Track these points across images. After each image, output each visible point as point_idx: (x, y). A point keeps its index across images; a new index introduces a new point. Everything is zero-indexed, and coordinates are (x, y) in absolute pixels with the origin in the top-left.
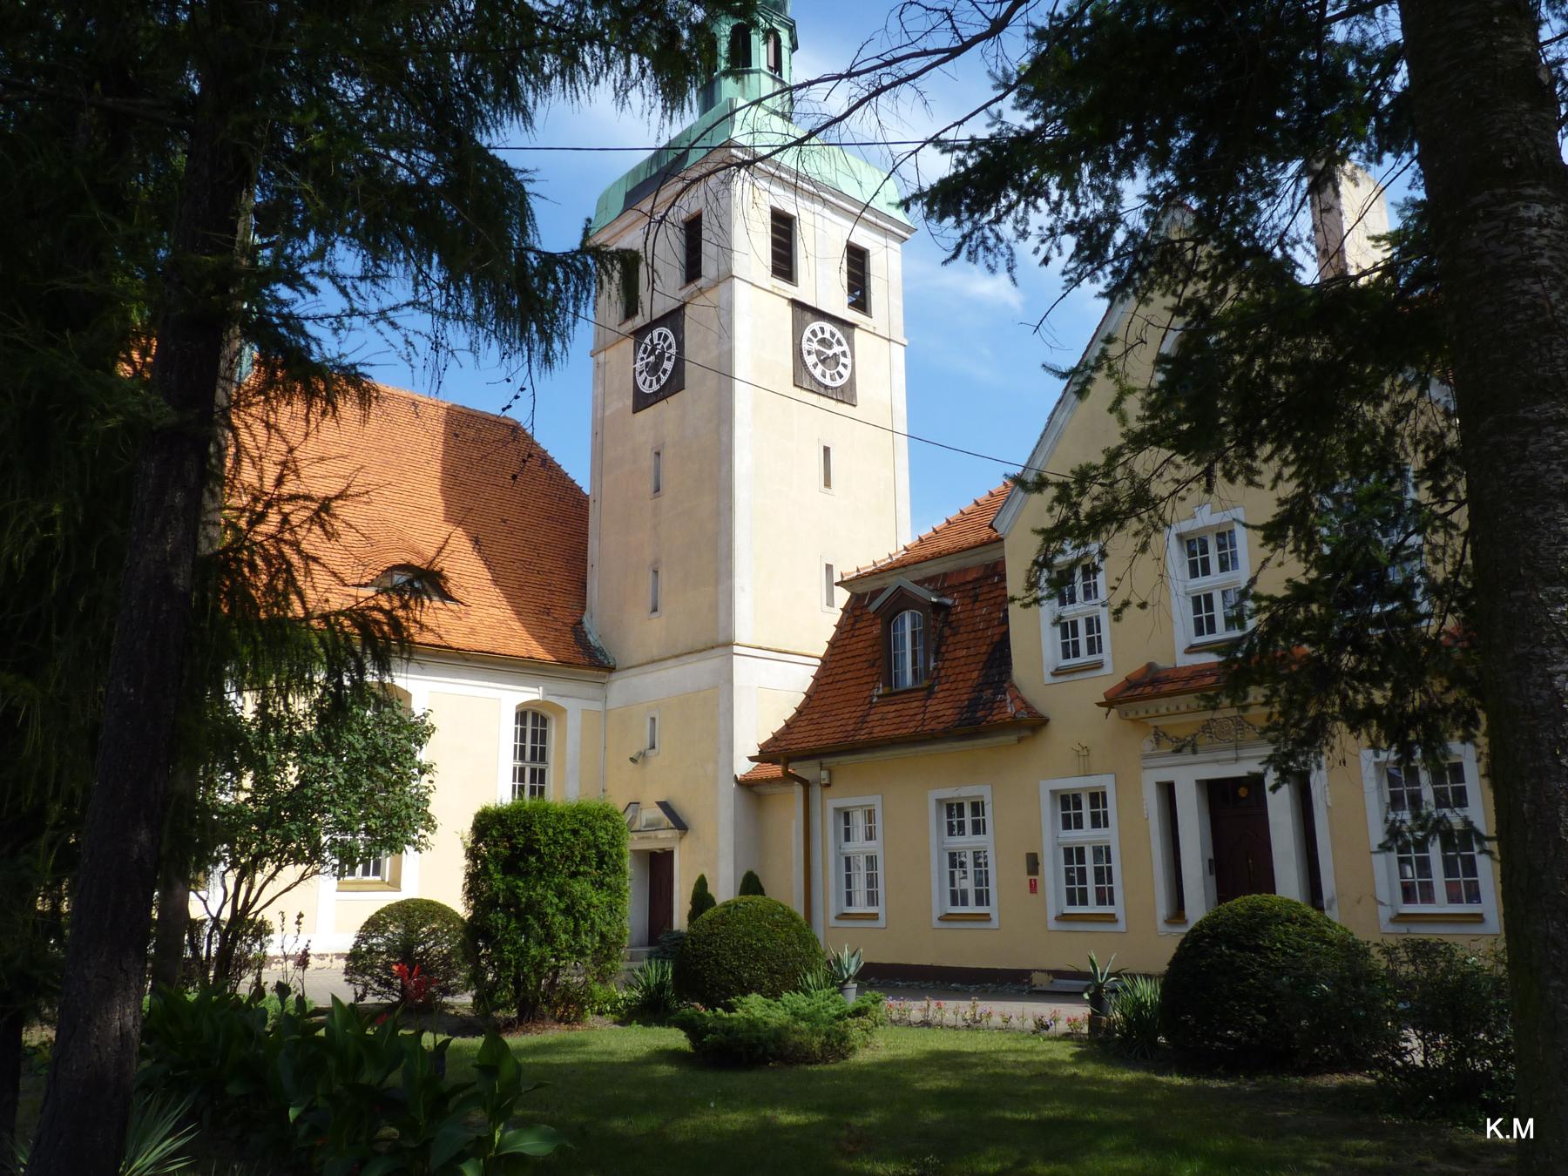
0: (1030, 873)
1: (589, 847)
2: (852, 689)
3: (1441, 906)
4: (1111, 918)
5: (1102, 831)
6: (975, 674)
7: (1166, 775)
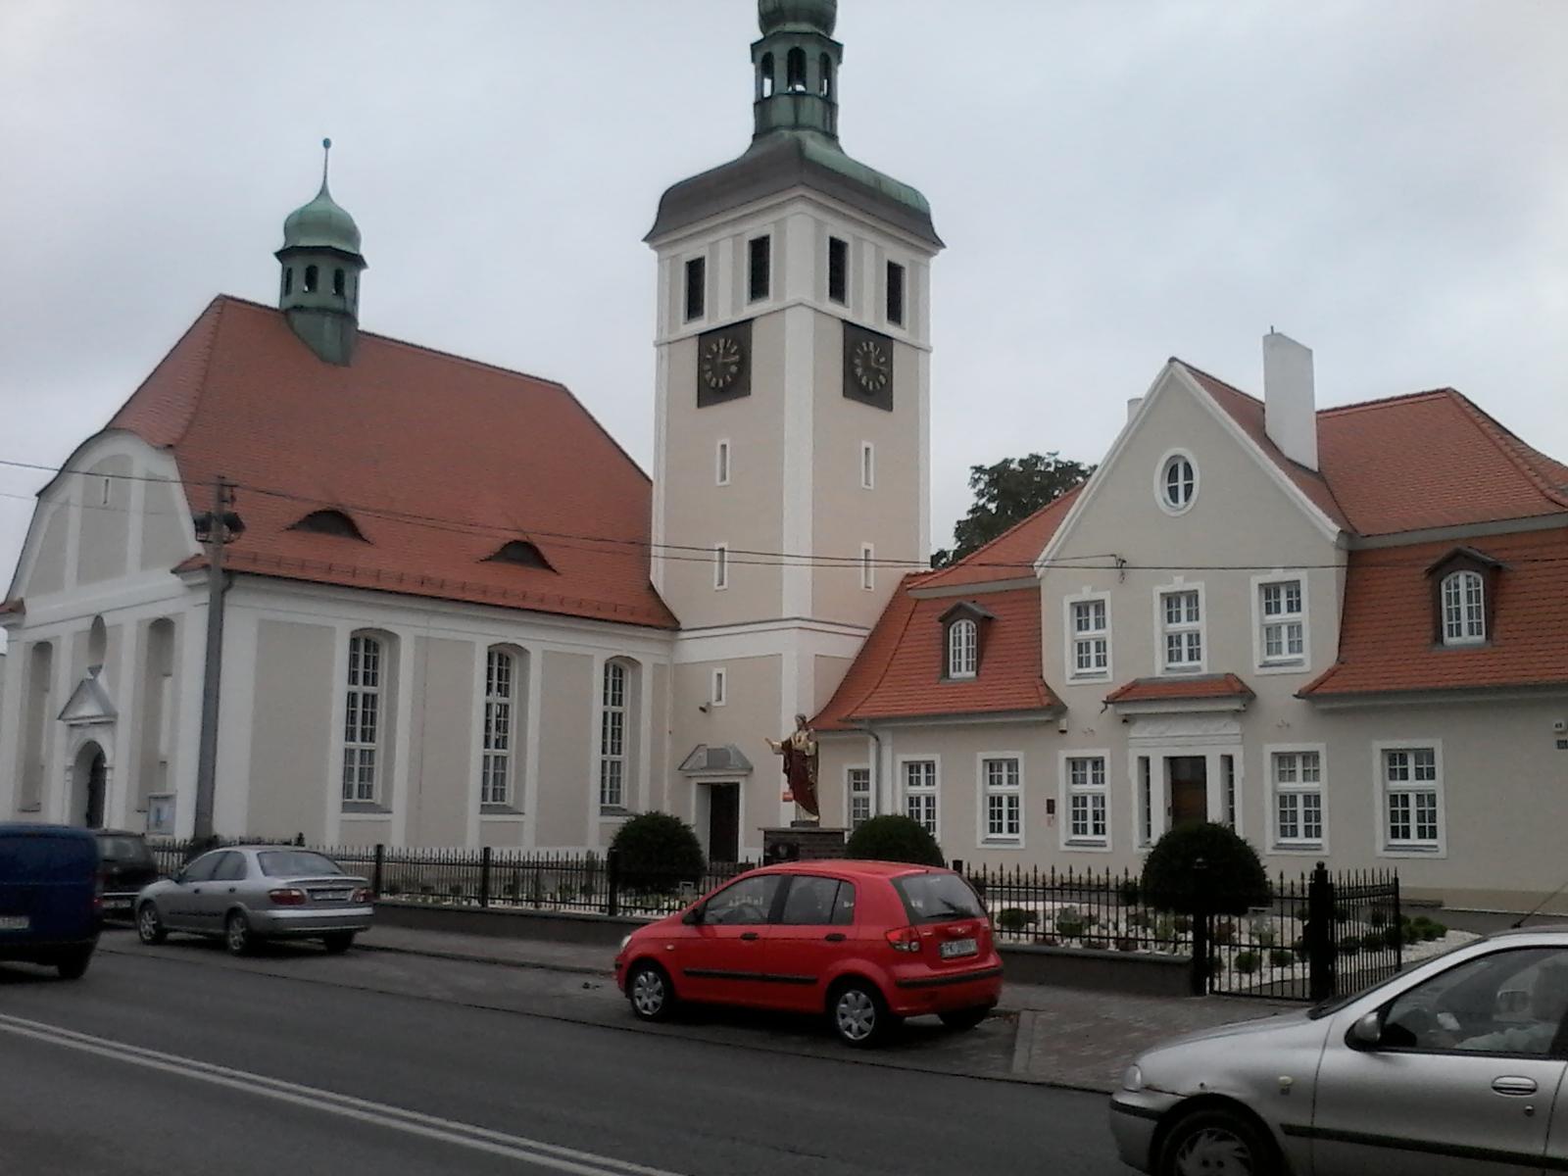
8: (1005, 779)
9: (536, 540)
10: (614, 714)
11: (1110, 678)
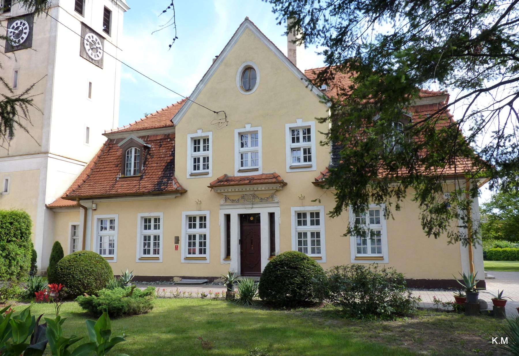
0: (176, 243)
1: (17, 230)
2: (108, 174)
3: (369, 254)
4: (204, 259)
5: (157, 231)
6: (160, 173)
7: (227, 212)
8: (198, 225)
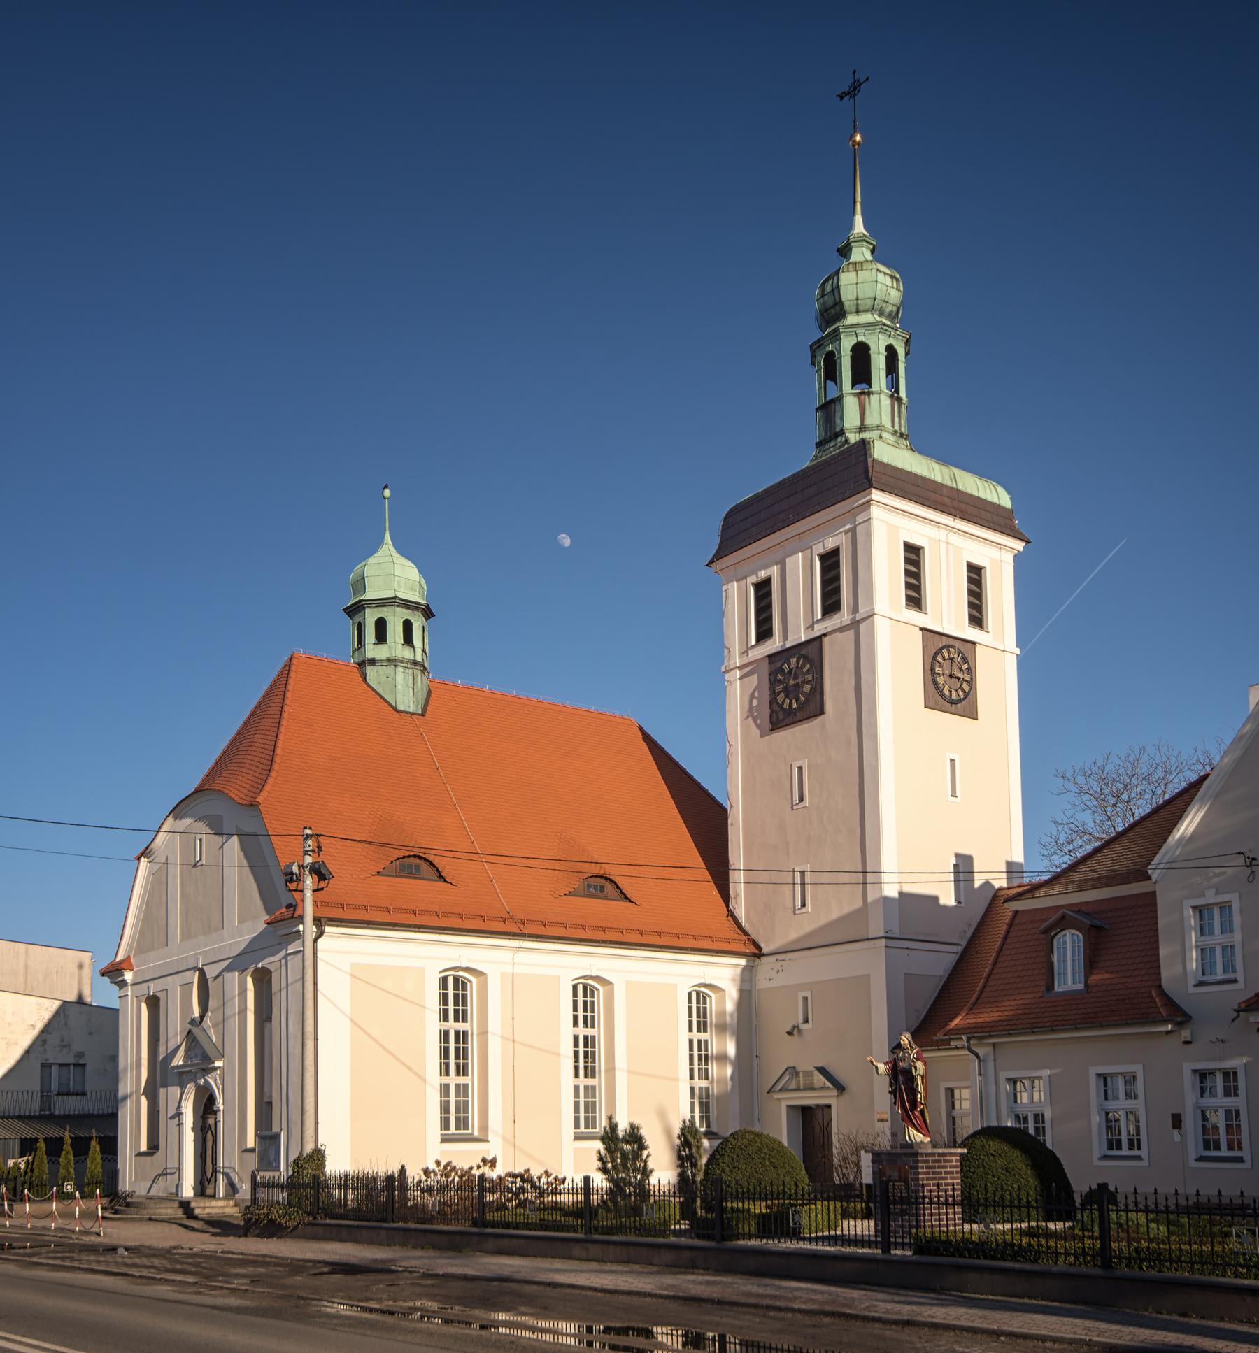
9: (611, 871)
10: (699, 1042)
11: (1240, 985)
